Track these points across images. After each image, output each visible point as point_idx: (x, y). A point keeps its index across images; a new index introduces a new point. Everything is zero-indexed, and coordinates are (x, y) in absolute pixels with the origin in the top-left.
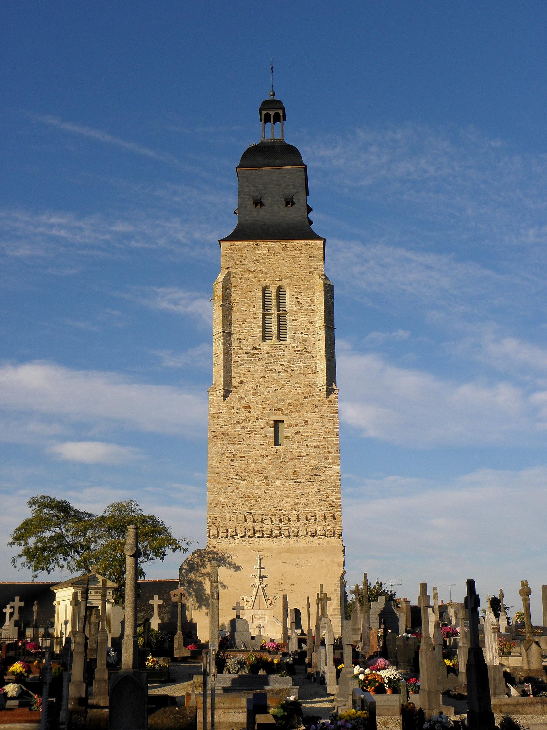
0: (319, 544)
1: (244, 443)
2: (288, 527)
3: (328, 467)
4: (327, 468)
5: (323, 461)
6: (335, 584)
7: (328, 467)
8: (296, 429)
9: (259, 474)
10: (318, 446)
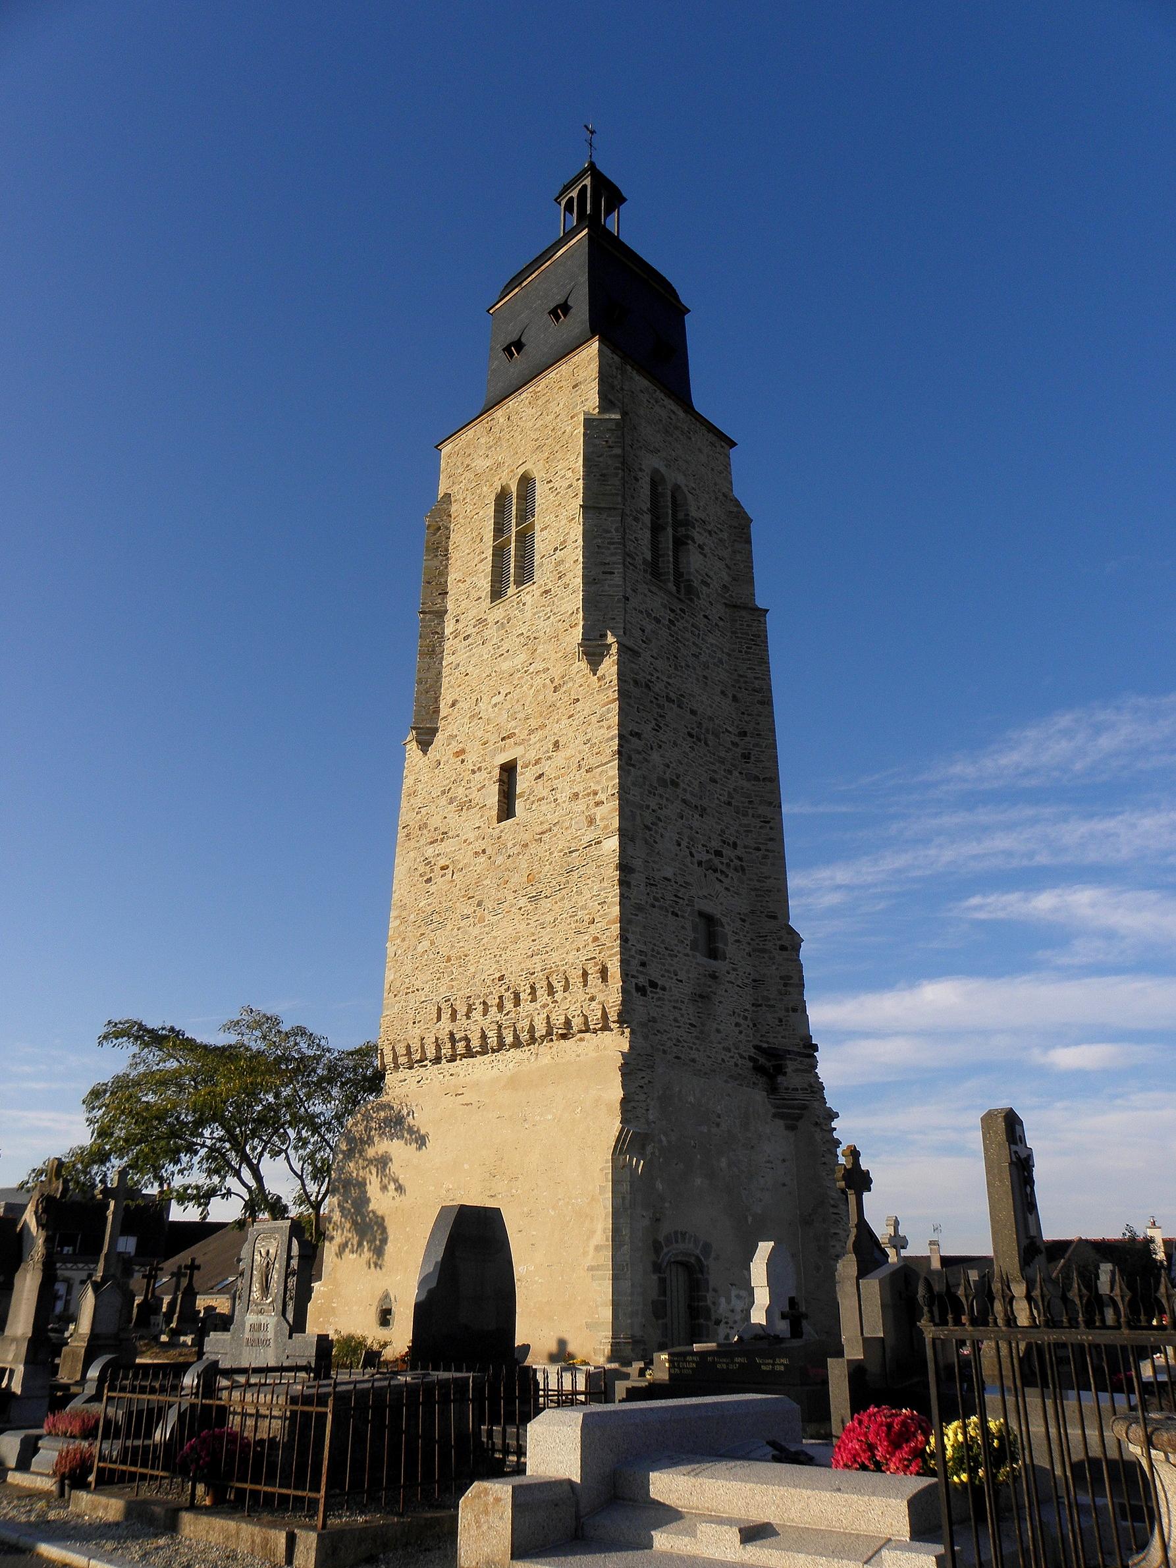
0: (578, 1056)
1: (450, 834)
2: (512, 1019)
3: (593, 843)
4: (591, 845)
5: (583, 831)
6: (601, 1170)
7: (593, 843)
8: (537, 770)
9: (469, 899)
10: (576, 795)
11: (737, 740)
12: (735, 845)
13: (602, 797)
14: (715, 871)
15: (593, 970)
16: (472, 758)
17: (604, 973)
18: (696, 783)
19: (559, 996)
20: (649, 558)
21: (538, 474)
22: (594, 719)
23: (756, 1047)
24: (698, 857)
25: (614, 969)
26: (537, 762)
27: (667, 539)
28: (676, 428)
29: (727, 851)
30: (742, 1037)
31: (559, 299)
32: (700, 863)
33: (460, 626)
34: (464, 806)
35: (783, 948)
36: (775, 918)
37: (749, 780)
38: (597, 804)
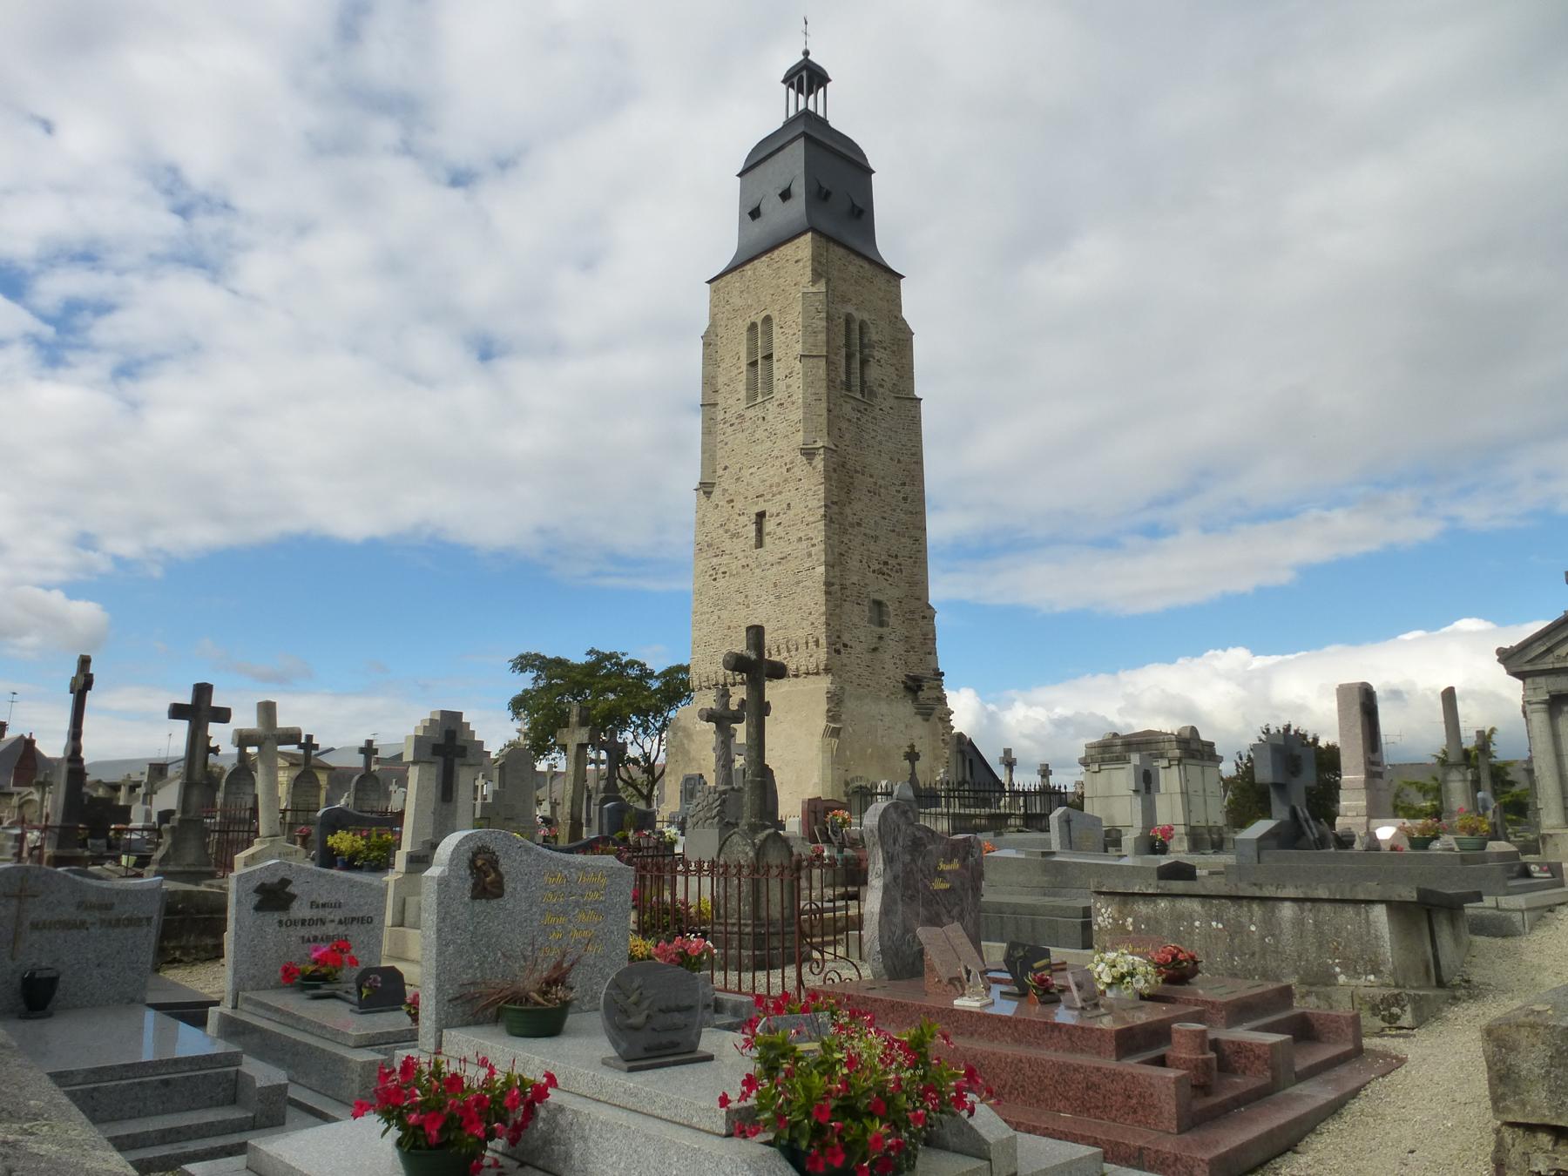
11: (899, 488)
12: (896, 556)
13: (814, 541)
14: (884, 574)
15: (811, 640)
16: (738, 505)
17: (817, 643)
18: (873, 522)
19: (793, 653)
20: (844, 379)
21: (775, 315)
22: (810, 493)
23: (906, 676)
24: (872, 568)
25: (823, 641)
26: (778, 515)
27: (856, 364)
28: (863, 278)
29: (892, 562)
30: (898, 670)
31: (784, 186)
32: (874, 571)
33: (727, 415)
34: (735, 535)
35: (924, 617)
36: (918, 599)
37: (906, 514)
38: (813, 545)
